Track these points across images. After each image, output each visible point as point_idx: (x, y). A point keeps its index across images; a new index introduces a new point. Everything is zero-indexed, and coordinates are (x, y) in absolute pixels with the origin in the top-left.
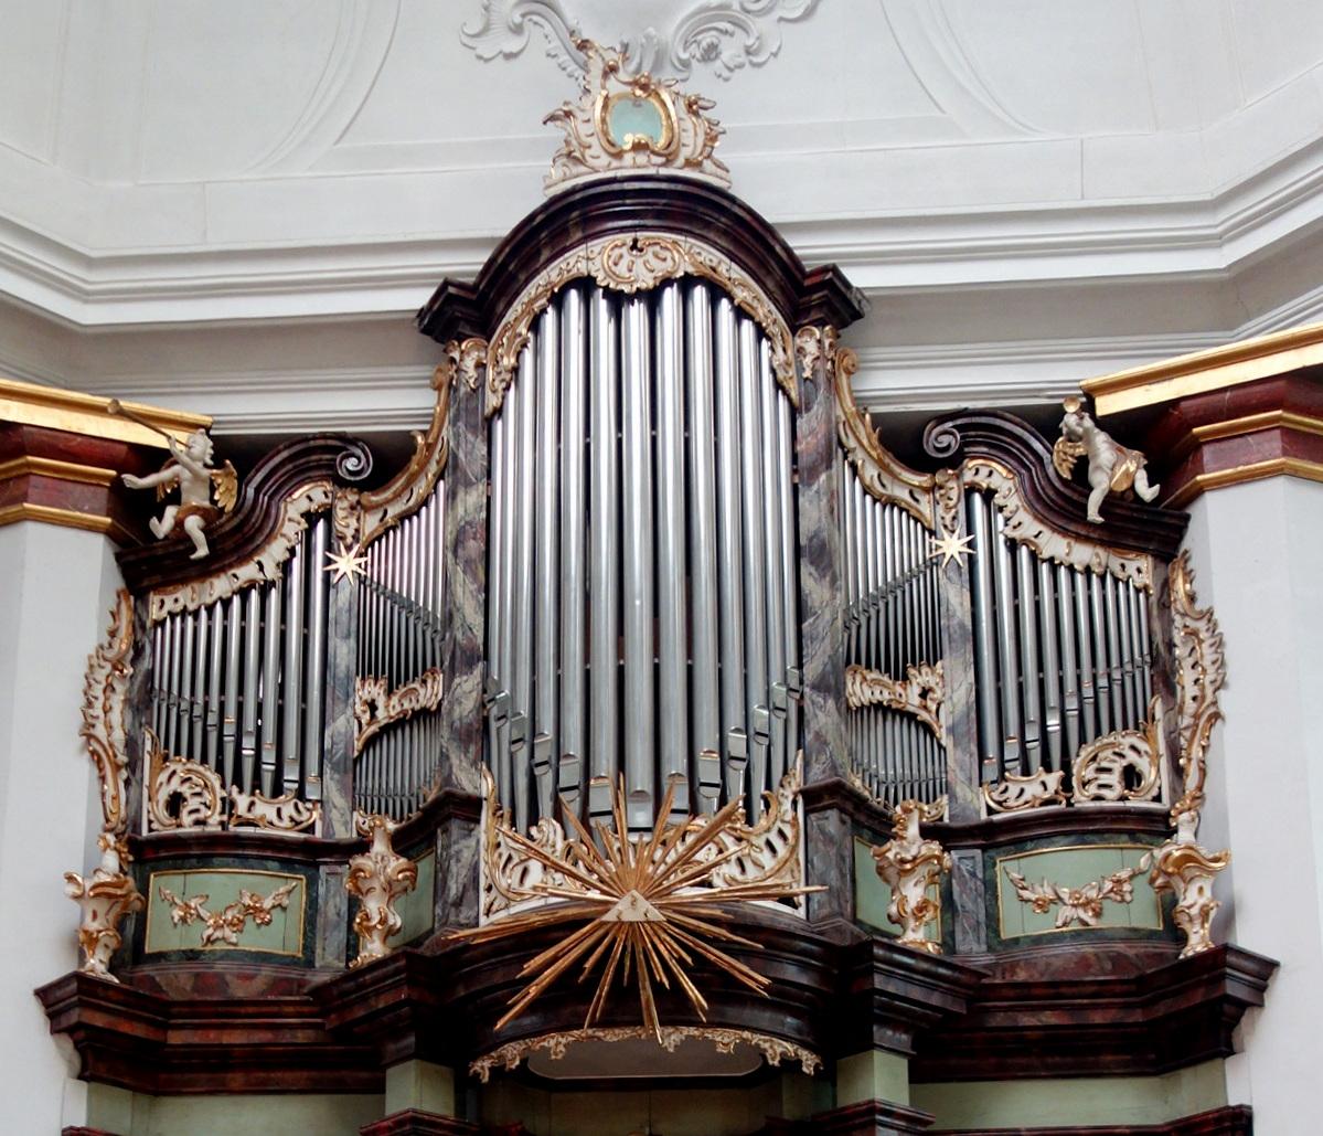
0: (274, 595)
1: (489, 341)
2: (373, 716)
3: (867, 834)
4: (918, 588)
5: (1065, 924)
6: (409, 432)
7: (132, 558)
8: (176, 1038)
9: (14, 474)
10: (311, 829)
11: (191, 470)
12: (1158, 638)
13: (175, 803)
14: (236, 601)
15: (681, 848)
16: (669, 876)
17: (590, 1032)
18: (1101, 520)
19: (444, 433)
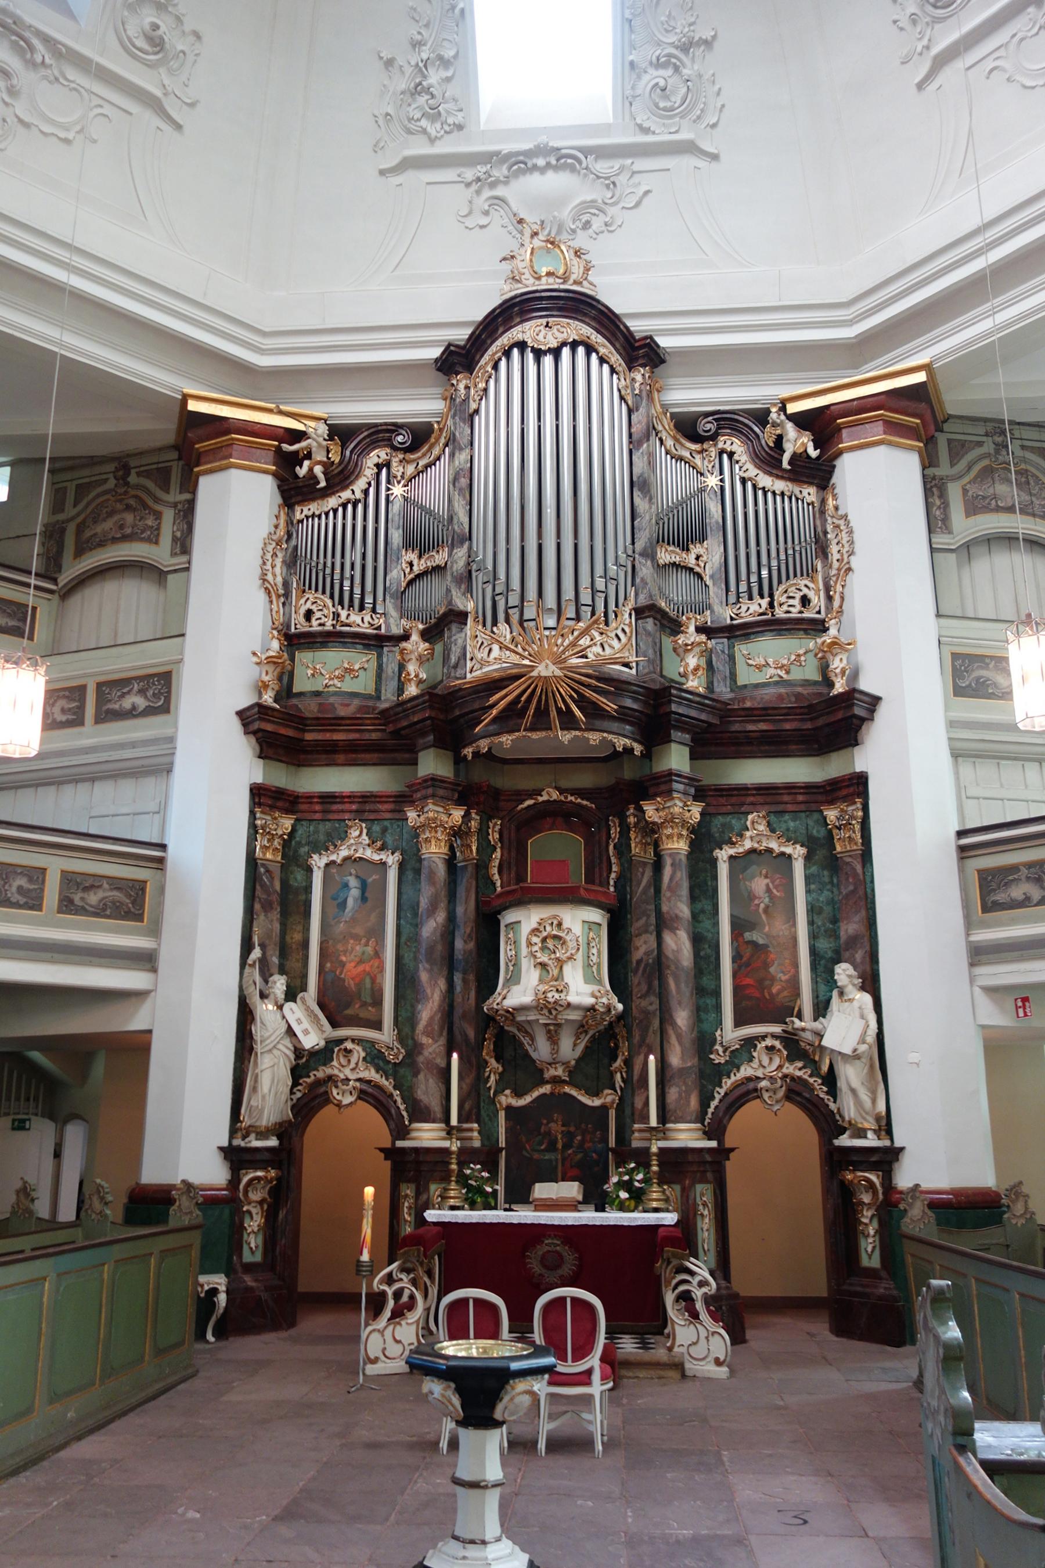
0: (360, 507)
2: (411, 569)
3: (668, 630)
4: (694, 503)
8: (309, 736)
10: (379, 628)
12: (819, 529)
13: (309, 614)
15: (571, 638)
16: (279, 799)
19: (448, 422)
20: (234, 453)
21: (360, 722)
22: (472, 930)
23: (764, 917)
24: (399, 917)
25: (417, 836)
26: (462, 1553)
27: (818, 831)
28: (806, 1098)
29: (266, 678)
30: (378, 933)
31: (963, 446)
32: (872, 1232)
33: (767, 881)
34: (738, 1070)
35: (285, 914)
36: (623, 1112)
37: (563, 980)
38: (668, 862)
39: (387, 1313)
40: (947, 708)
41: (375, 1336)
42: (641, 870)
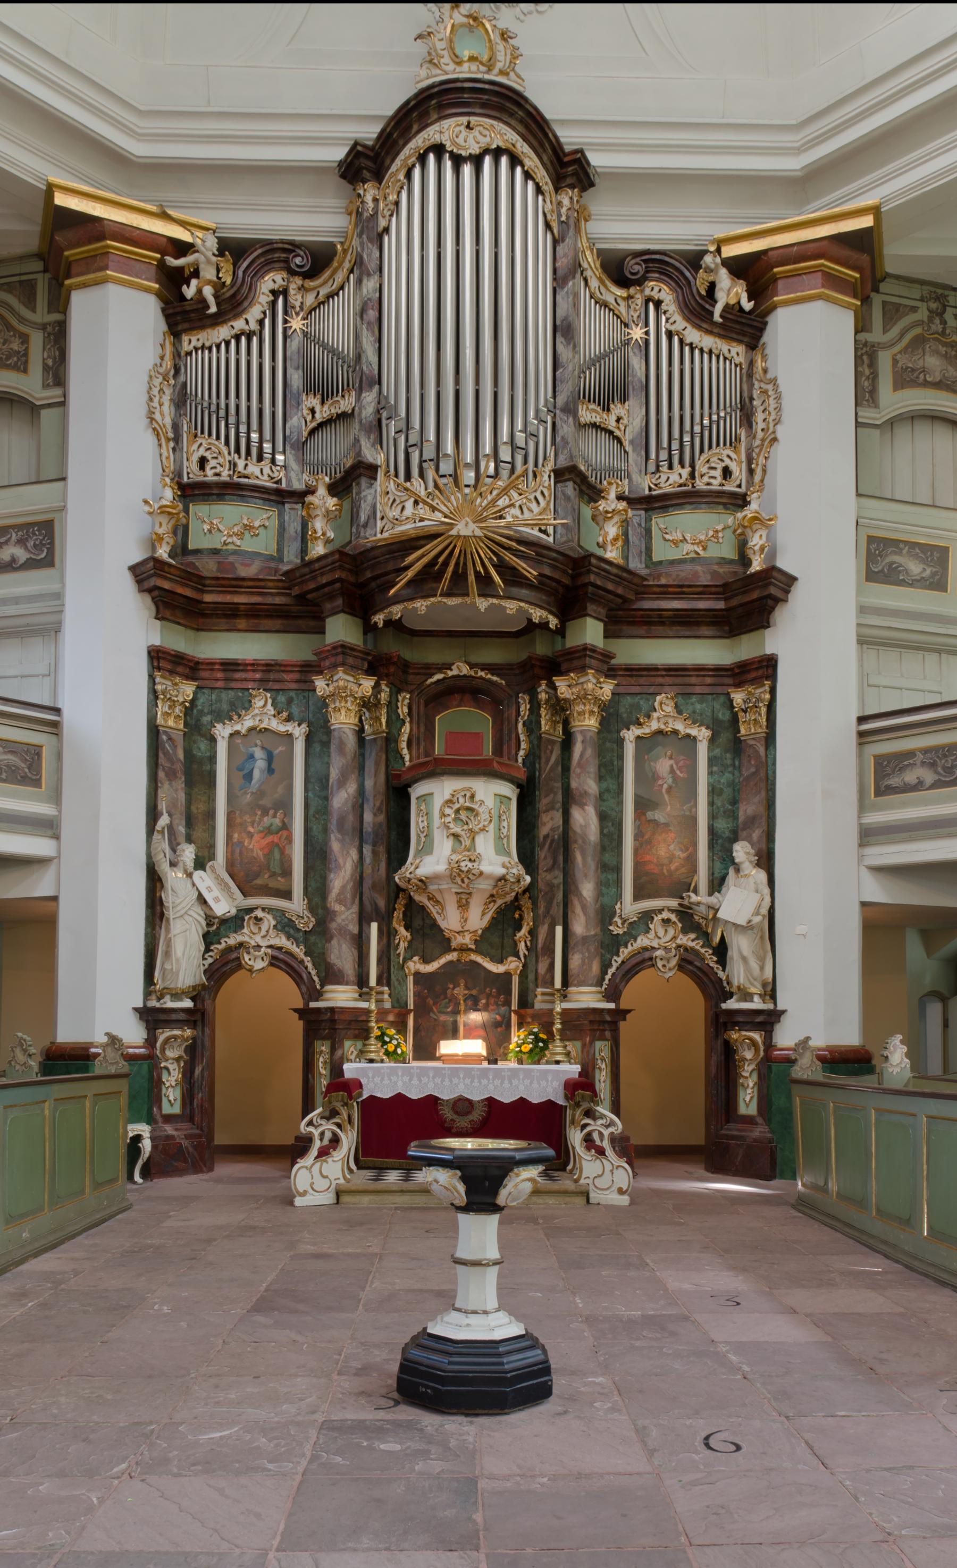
1: (380, 184)
2: (313, 417)
3: (586, 497)
4: (617, 358)
5: (687, 554)
6: (332, 242)
7: (171, 311)
8: (208, 598)
9: (100, 252)
10: (279, 482)
11: (205, 257)
12: (746, 395)
13: (203, 462)
14: (233, 342)
15: (490, 498)
16: (180, 664)
17: (440, 599)
18: (720, 320)
19: (354, 243)
20: (110, 264)
21: (262, 584)
22: (381, 804)
23: (666, 797)
24: (306, 790)
25: (327, 706)
26: (467, 1321)
27: (723, 714)
28: (696, 967)
29: (160, 531)
30: (285, 805)
31: (897, 310)
32: (751, 1084)
33: (672, 762)
34: (635, 940)
35: (190, 784)
36: (527, 978)
37: (475, 850)
38: (579, 738)
39: (314, 1152)
40: (859, 592)
41: (303, 1172)
42: (550, 747)
